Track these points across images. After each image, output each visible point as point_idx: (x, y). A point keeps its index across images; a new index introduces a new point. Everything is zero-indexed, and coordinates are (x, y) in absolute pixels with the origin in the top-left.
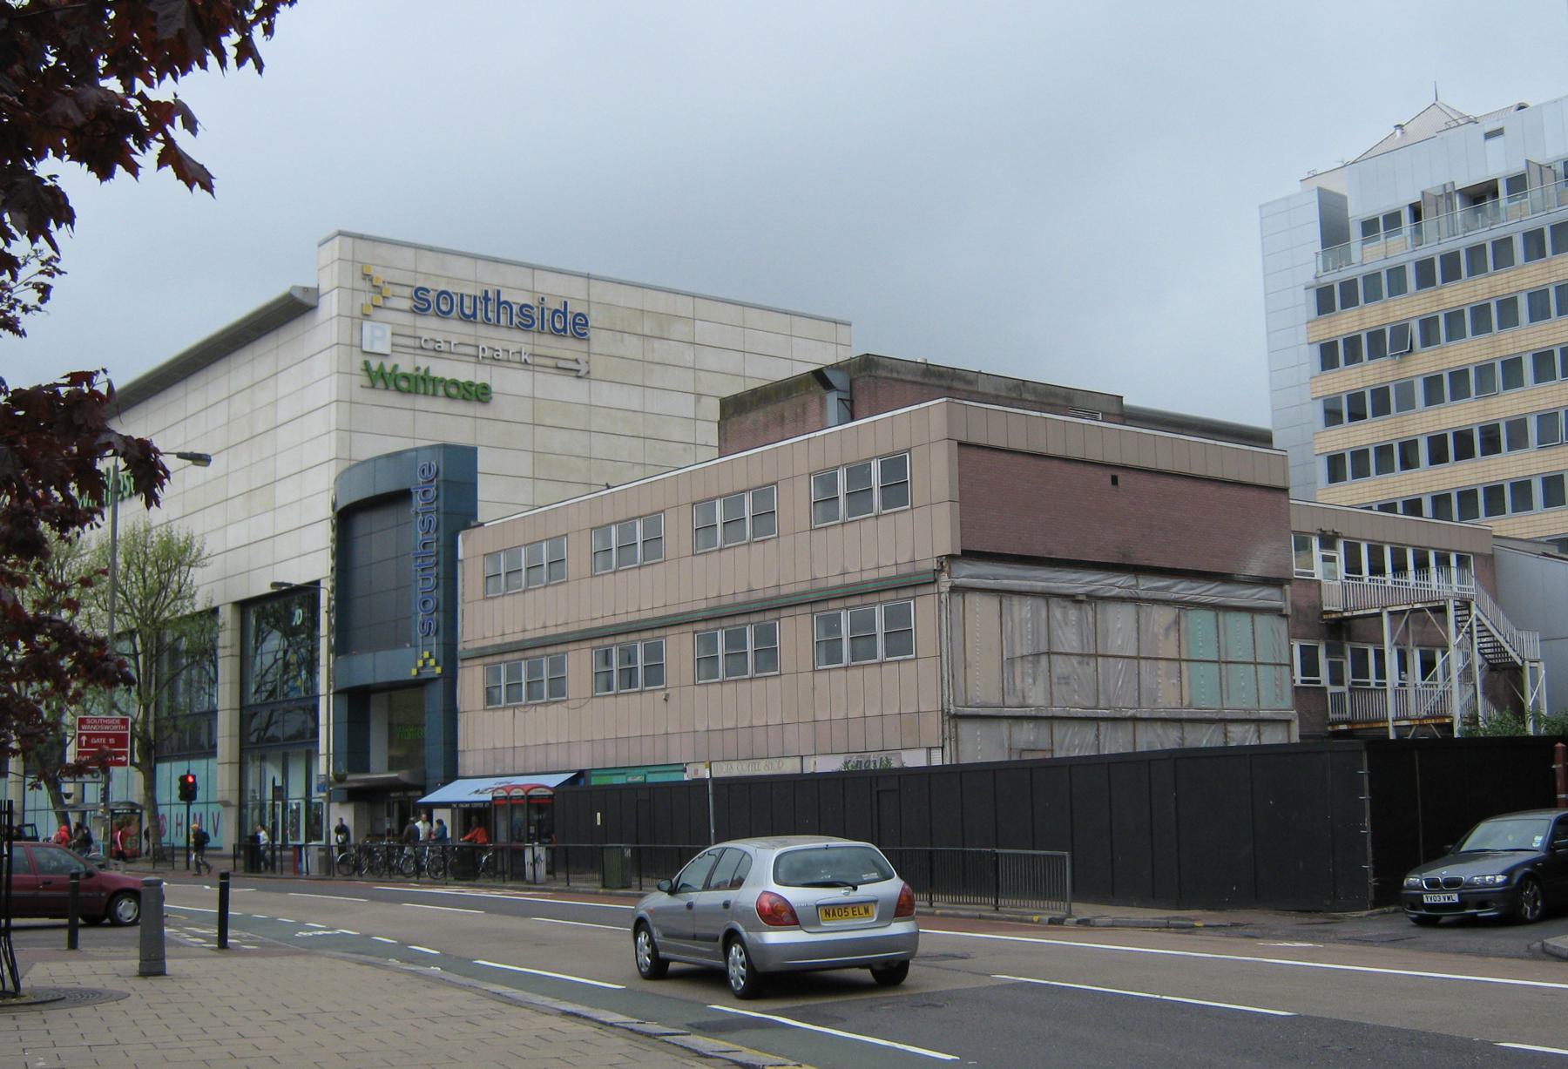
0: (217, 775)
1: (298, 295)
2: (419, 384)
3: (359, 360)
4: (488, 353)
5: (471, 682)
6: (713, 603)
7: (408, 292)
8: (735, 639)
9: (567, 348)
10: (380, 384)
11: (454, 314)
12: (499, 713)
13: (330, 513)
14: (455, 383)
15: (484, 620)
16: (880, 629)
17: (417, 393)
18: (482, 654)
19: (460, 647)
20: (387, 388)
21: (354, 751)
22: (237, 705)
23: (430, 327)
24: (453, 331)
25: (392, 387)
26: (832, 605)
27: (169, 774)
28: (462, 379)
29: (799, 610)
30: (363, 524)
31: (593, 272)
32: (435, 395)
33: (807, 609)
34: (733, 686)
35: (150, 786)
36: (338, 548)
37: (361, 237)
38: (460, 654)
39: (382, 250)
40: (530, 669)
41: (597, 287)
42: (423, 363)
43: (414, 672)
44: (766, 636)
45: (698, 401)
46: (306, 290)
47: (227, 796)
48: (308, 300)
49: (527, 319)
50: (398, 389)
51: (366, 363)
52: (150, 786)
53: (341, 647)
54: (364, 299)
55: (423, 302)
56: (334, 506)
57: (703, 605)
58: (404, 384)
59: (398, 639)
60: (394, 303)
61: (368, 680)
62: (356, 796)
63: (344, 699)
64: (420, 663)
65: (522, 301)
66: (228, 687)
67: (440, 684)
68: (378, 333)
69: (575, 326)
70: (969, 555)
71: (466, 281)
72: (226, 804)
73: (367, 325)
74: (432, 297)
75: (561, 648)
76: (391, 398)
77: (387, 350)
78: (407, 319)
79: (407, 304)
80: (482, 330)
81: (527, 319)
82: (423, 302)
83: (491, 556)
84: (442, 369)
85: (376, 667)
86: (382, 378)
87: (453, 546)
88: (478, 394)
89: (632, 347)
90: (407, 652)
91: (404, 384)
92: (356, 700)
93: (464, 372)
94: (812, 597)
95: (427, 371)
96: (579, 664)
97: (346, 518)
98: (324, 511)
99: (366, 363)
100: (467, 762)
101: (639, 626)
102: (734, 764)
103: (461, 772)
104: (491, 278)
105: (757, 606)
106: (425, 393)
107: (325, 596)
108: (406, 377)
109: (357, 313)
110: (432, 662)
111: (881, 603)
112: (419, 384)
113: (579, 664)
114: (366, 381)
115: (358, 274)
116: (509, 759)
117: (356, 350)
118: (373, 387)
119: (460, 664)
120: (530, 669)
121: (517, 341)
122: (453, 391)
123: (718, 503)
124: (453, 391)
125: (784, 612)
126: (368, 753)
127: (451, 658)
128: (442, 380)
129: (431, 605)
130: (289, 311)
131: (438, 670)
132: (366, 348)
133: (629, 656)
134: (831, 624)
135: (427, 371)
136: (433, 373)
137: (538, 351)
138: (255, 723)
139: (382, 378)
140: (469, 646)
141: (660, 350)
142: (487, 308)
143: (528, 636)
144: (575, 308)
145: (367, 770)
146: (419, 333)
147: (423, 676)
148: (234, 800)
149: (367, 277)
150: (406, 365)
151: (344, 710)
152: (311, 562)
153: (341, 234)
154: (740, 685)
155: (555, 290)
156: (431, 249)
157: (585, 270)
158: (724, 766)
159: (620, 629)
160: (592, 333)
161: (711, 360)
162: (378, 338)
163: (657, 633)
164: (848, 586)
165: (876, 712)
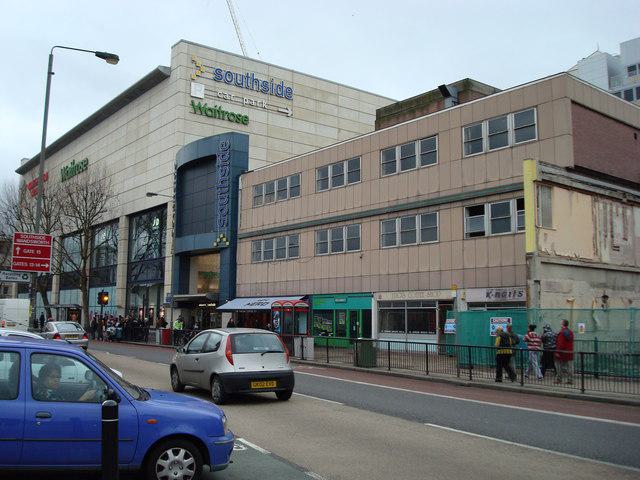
0: (116, 295)
2: (216, 114)
3: (190, 100)
5: (245, 249)
6: (395, 203)
8: (409, 223)
9: (282, 103)
10: (198, 112)
12: (260, 265)
13: (174, 171)
15: (253, 218)
16: (418, 227)
18: (251, 235)
19: (239, 232)
21: (182, 283)
23: (221, 88)
24: (232, 91)
26: (410, 212)
27: (94, 293)
29: (372, 218)
33: (460, 204)
34: (406, 249)
35: (86, 299)
36: (177, 222)
37: (192, 43)
38: (239, 236)
39: (201, 50)
40: (280, 243)
41: (296, 77)
42: (219, 104)
43: (215, 244)
44: (430, 219)
45: (339, 132)
46: (165, 68)
47: (120, 303)
49: (265, 88)
51: (192, 102)
52: (86, 299)
53: (179, 232)
55: (219, 76)
56: (176, 166)
57: (386, 205)
59: (207, 228)
61: (191, 248)
63: (178, 258)
64: (218, 240)
69: (288, 94)
70: (577, 169)
71: (240, 70)
72: (119, 307)
74: (223, 73)
75: (296, 231)
76: (203, 119)
78: (212, 83)
79: (212, 76)
81: (265, 88)
82: (219, 76)
83: (258, 187)
84: (227, 108)
85: (192, 243)
86: (199, 109)
87: (236, 183)
88: (244, 120)
89: (311, 105)
90: (212, 235)
91: (209, 113)
92: (184, 259)
93: (237, 110)
94: (463, 197)
96: (307, 240)
97: (182, 172)
98: (171, 170)
99: (192, 102)
100: (241, 290)
101: (449, 200)
102: (406, 293)
103: (238, 295)
104: (250, 69)
105: (424, 204)
107: (170, 211)
110: (224, 239)
112: (216, 114)
113: (307, 240)
114: (191, 109)
115: (190, 61)
116: (265, 288)
119: (238, 241)
120: (280, 243)
121: (261, 98)
122: (232, 118)
123: (397, 148)
124: (232, 118)
125: (442, 207)
127: (234, 238)
129: (224, 212)
131: (228, 243)
133: (338, 234)
134: (323, 236)
138: (135, 272)
139: (199, 109)
140: (244, 232)
141: (324, 107)
142: (247, 82)
143: (277, 225)
144: (286, 85)
145: (187, 293)
148: (124, 306)
150: (211, 105)
151: (178, 262)
152: (166, 193)
153: (182, 41)
154: (410, 249)
155: (278, 77)
158: (389, 294)
159: (431, 203)
161: (345, 114)
162: (198, 90)
163: (356, 221)
165: (497, 263)
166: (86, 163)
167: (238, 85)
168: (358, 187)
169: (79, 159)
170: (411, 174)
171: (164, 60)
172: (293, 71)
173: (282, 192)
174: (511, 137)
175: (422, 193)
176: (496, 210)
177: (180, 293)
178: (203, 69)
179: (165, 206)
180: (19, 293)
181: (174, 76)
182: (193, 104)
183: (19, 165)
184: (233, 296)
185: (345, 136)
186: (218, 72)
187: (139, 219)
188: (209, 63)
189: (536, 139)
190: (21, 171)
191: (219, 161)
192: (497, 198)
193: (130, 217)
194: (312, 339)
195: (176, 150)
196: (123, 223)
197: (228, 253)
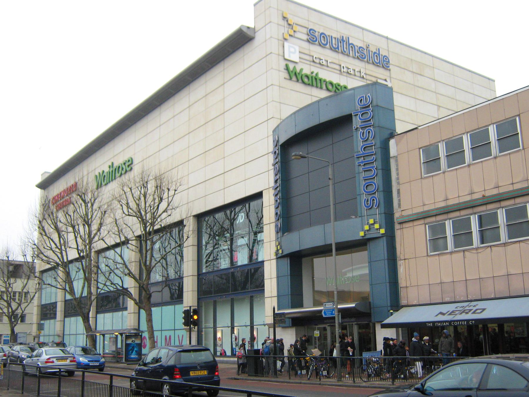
1: (245, 30)
3: (283, 64)
4: (345, 70)
5: (412, 241)
7: (305, 31)
10: (294, 78)
11: (328, 46)
13: (271, 147)
14: (331, 84)
17: (312, 85)
19: (397, 215)
20: (298, 81)
21: (293, 292)
22: (196, 274)
23: (316, 51)
24: (327, 55)
25: (300, 81)
28: (335, 82)
29: (416, 223)
30: (295, 152)
31: (389, 37)
32: (321, 88)
33: (422, 222)
42: (315, 70)
45: (438, 110)
46: (248, 28)
48: (250, 33)
50: (303, 82)
53: (286, 223)
54: (284, 30)
55: (313, 38)
58: (306, 80)
59: (347, 209)
60: (298, 35)
62: (297, 322)
63: (287, 262)
65: (359, 45)
66: (191, 263)
67: (384, 240)
68: (292, 50)
71: (335, 31)
73: (286, 44)
76: (299, 86)
77: (297, 59)
78: (306, 45)
80: (341, 56)
82: (313, 38)
86: (294, 75)
89: (408, 77)
90: (354, 221)
91: (306, 80)
92: (296, 262)
95: (317, 74)
97: (288, 149)
103: (403, 302)
106: (317, 87)
108: (307, 76)
109: (281, 38)
110: (377, 226)
111: (450, 219)
114: (287, 76)
115: (281, 18)
117: (281, 58)
118: (291, 79)
123: (465, 137)
126: (302, 295)
128: (325, 81)
130: (240, 40)
132: (287, 57)
135: (317, 74)
136: (321, 76)
137: (368, 72)
139: (294, 75)
145: (301, 306)
146: (312, 54)
147: (368, 236)
149: (284, 18)
150: (307, 70)
152: (262, 177)
155: (374, 44)
156: (315, 10)
157: (386, 35)
160: (391, 67)
162: (293, 51)
164: (502, 194)
166: (129, 164)
167: (335, 50)
168: (515, 158)
169: (118, 161)
170: (487, 163)
171: (247, 21)
172: (387, 38)
173: (481, 148)
174: (443, 162)
175: (476, 191)
176: (456, 225)
177: (293, 307)
178: (296, 28)
179: (259, 195)
180: (65, 316)
181: (259, 38)
182: (287, 68)
183: (39, 180)
184: (396, 306)
185: (444, 113)
186: (311, 32)
187: (217, 222)
188: (300, 22)
189: (521, 148)
190: (44, 185)
191: (357, 122)
192: (457, 214)
193: (200, 217)
194: (334, 356)
195: (273, 124)
196: (190, 226)
197: (381, 247)
